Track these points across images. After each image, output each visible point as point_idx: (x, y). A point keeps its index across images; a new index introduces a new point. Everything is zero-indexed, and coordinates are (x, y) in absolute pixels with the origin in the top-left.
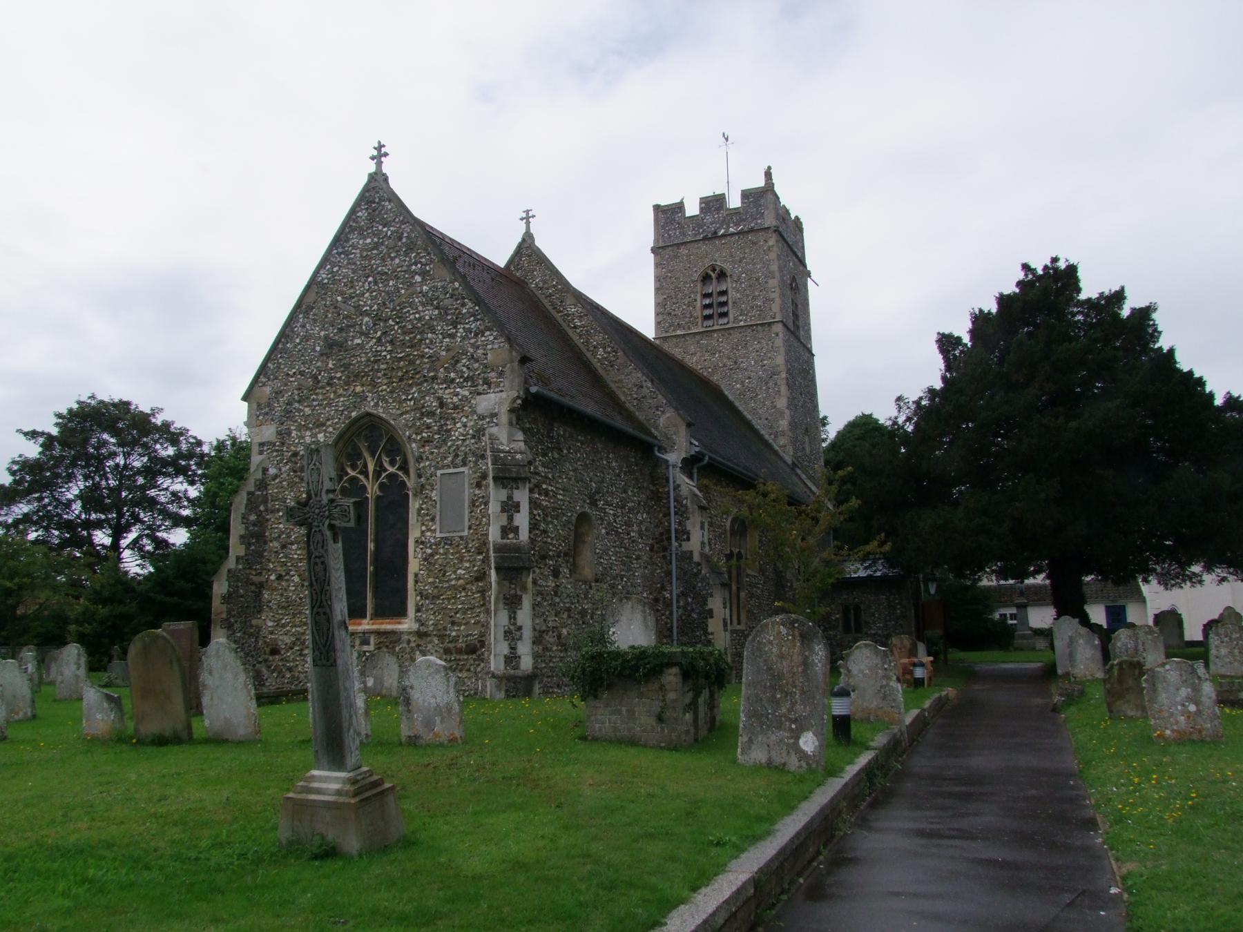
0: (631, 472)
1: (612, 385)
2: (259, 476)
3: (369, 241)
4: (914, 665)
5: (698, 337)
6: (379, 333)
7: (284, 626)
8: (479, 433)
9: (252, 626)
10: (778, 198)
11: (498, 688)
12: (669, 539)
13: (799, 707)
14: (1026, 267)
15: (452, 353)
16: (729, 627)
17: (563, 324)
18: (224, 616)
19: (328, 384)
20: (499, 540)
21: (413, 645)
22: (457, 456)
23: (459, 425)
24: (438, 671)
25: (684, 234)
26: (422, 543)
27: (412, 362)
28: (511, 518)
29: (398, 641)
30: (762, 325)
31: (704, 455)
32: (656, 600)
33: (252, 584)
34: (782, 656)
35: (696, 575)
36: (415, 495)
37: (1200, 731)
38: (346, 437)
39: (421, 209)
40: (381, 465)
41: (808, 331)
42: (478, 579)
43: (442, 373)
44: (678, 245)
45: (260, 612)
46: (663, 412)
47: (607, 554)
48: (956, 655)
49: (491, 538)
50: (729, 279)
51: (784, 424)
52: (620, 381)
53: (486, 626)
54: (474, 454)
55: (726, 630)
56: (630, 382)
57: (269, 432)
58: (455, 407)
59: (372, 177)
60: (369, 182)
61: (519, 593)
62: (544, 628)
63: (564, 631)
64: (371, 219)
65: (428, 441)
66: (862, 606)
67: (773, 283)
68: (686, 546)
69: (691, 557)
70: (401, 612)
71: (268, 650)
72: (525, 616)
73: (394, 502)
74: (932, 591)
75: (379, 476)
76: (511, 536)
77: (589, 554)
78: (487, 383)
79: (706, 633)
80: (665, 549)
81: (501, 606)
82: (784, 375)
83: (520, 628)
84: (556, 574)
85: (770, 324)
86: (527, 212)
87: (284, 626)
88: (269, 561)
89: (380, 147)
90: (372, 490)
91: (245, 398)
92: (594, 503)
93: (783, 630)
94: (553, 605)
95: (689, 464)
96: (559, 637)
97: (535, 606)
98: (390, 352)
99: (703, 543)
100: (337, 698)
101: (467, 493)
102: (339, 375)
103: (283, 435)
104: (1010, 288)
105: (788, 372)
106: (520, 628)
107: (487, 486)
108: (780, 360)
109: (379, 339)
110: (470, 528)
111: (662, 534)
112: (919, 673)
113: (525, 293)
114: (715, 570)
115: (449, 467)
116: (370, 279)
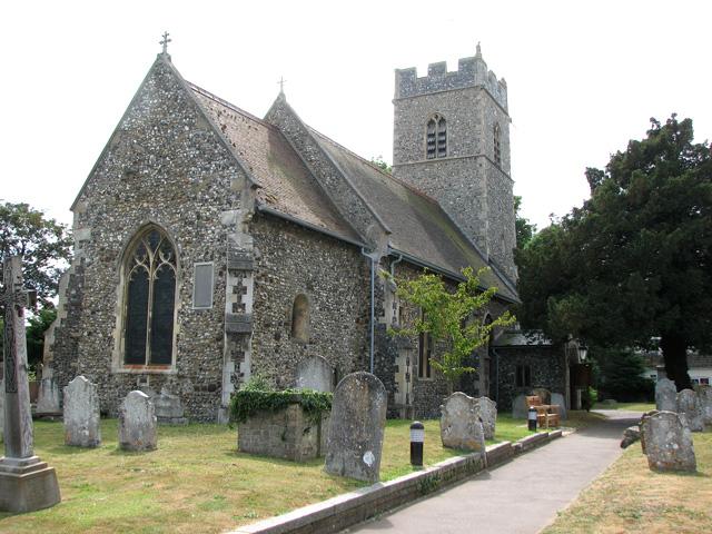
0: (345, 266)
1: (335, 203)
11: (225, 415)
12: (370, 315)
13: (364, 435)
14: (653, 120)
18: (51, 359)
22: (207, 253)
27: (180, 187)
28: (240, 298)
29: (165, 380)
32: (360, 358)
34: (355, 400)
35: (388, 341)
37: (680, 463)
45: (76, 357)
49: (226, 312)
52: (341, 200)
58: (208, 219)
59: (160, 57)
63: (283, 378)
68: (382, 320)
73: (166, 283)
78: (229, 203)
80: (367, 322)
83: (242, 375)
84: (277, 337)
85: (476, 158)
90: (152, 275)
91: (71, 210)
92: (310, 288)
93: (358, 383)
96: (278, 382)
99: (394, 318)
100: (18, 412)
101: (213, 279)
103: (95, 235)
104: (641, 136)
109: (160, 171)
111: (365, 311)
115: (201, 260)
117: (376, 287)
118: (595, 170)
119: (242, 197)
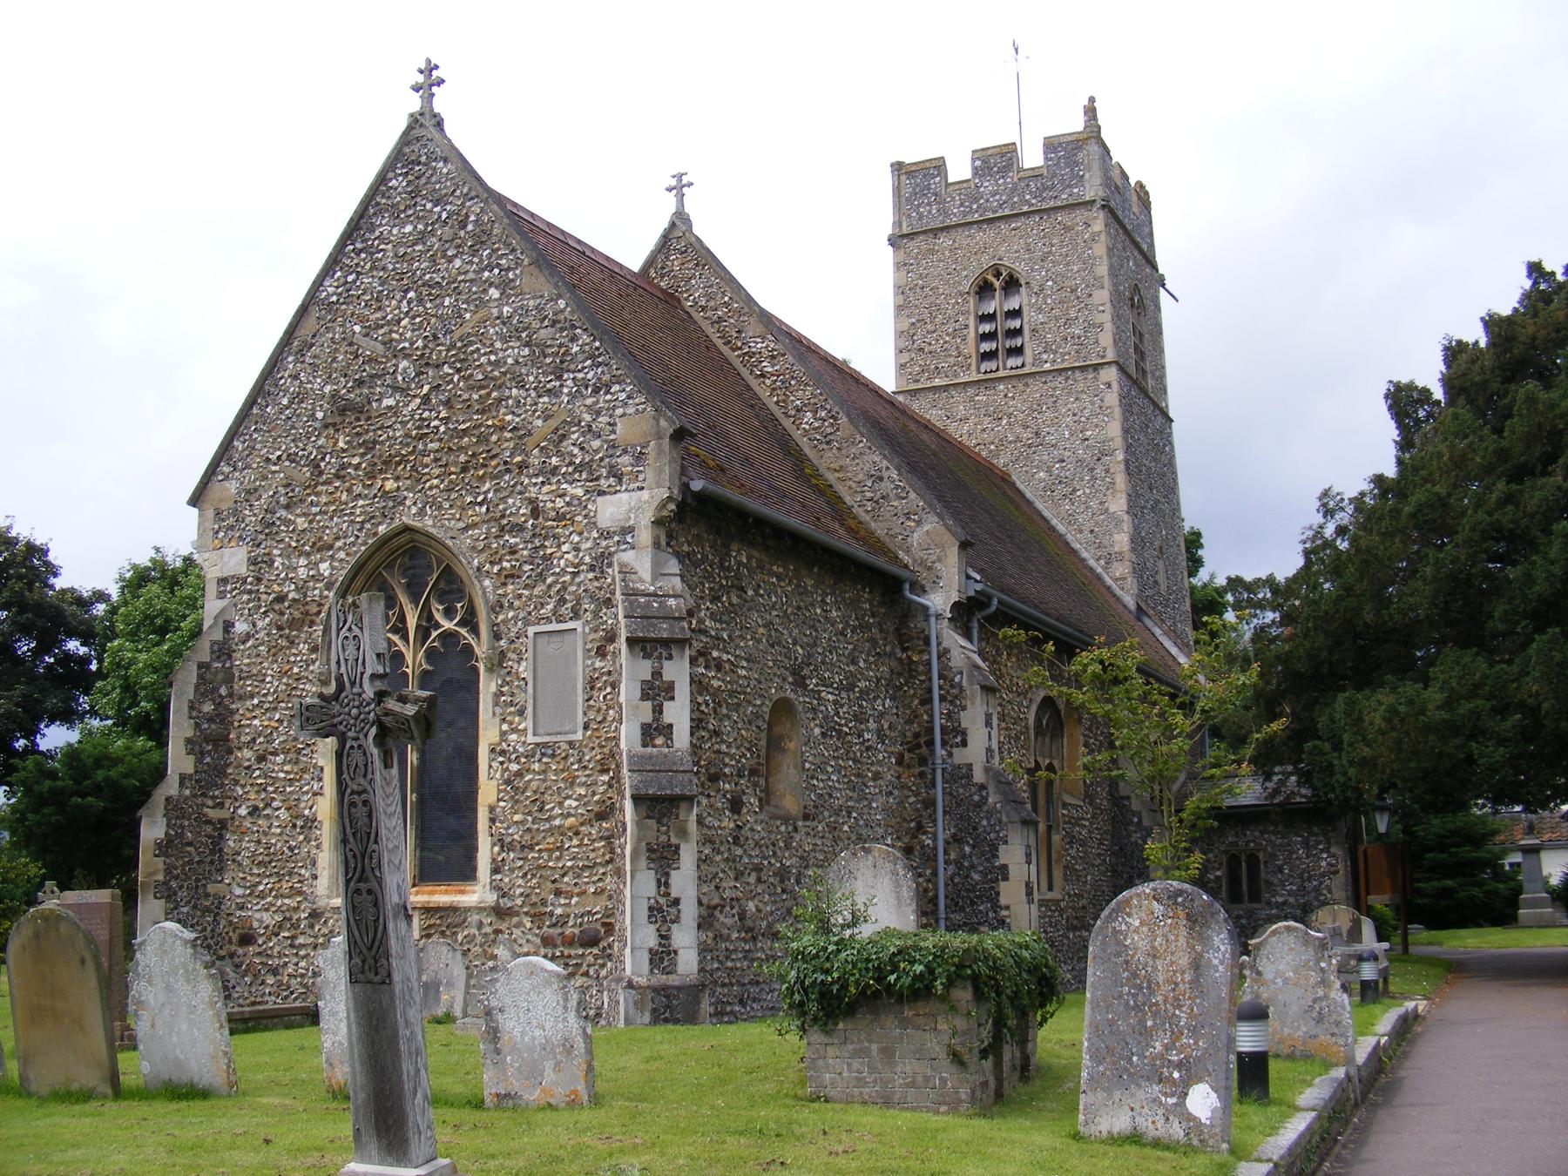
0: (865, 627)
1: (831, 477)
2: (218, 635)
3: (409, 228)
4: (1360, 959)
5: (971, 391)
6: (426, 388)
7: (262, 896)
8: (601, 562)
9: (207, 895)
10: (1108, 151)
12: (930, 743)
15: (553, 423)
16: (1036, 896)
17: (745, 372)
18: (160, 877)
19: (337, 476)
20: (639, 749)
21: (488, 930)
22: (562, 601)
23: (565, 548)
24: (548, 983)
25: (945, 212)
26: (503, 753)
28: (658, 710)
29: (462, 924)
30: (1083, 369)
31: (990, 598)
33: (209, 822)
35: (979, 805)
36: (490, 670)
38: (371, 566)
39: (505, 174)
40: (430, 617)
41: (1161, 379)
42: (601, 816)
43: (535, 459)
44: (936, 232)
45: (220, 870)
46: (919, 523)
47: (824, 771)
48: (1420, 935)
50: (1023, 290)
51: (1122, 541)
53: (615, 896)
54: (593, 598)
55: (1031, 901)
56: (861, 473)
57: (235, 560)
58: (560, 517)
59: (415, 121)
60: (410, 128)
61: (674, 840)
62: (716, 901)
63: (751, 906)
64: (414, 194)
65: (512, 576)
66: (1261, 855)
67: (1102, 296)
68: (960, 756)
69: (969, 776)
70: (464, 872)
71: (235, 938)
72: (684, 881)
73: (453, 678)
74: (1382, 828)
75: (426, 635)
76: (659, 741)
77: (792, 771)
79: (996, 906)
80: (923, 761)
81: (643, 863)
82: (1120, 456)
84: (736, 805)
85: (1096, 367)
86: (680, 176)
87: (262, 896)
88: (236, 782)
89: (430, 68)
92: (800, 683)
93: (1158, 908)
94: (731, 860)
95: (964, 613)
97: (702, 861)
98: (446, 420)
99: (989, 750)
100: (394, 1039)
102: (356, 461)
104: (1506, 303)
105: (1128, 449)
106: (676, 902)
107: (616, 654)
108: (1114, 429)
109: (426, 399)
110: (586, 727)
111: (917, 735)
112: (1368, 971)
113: (667, 322)
114: (1014, 801)
116: (411, 294)
117: (941, 677)
118: (1411, 387)
119: (651, 459)
